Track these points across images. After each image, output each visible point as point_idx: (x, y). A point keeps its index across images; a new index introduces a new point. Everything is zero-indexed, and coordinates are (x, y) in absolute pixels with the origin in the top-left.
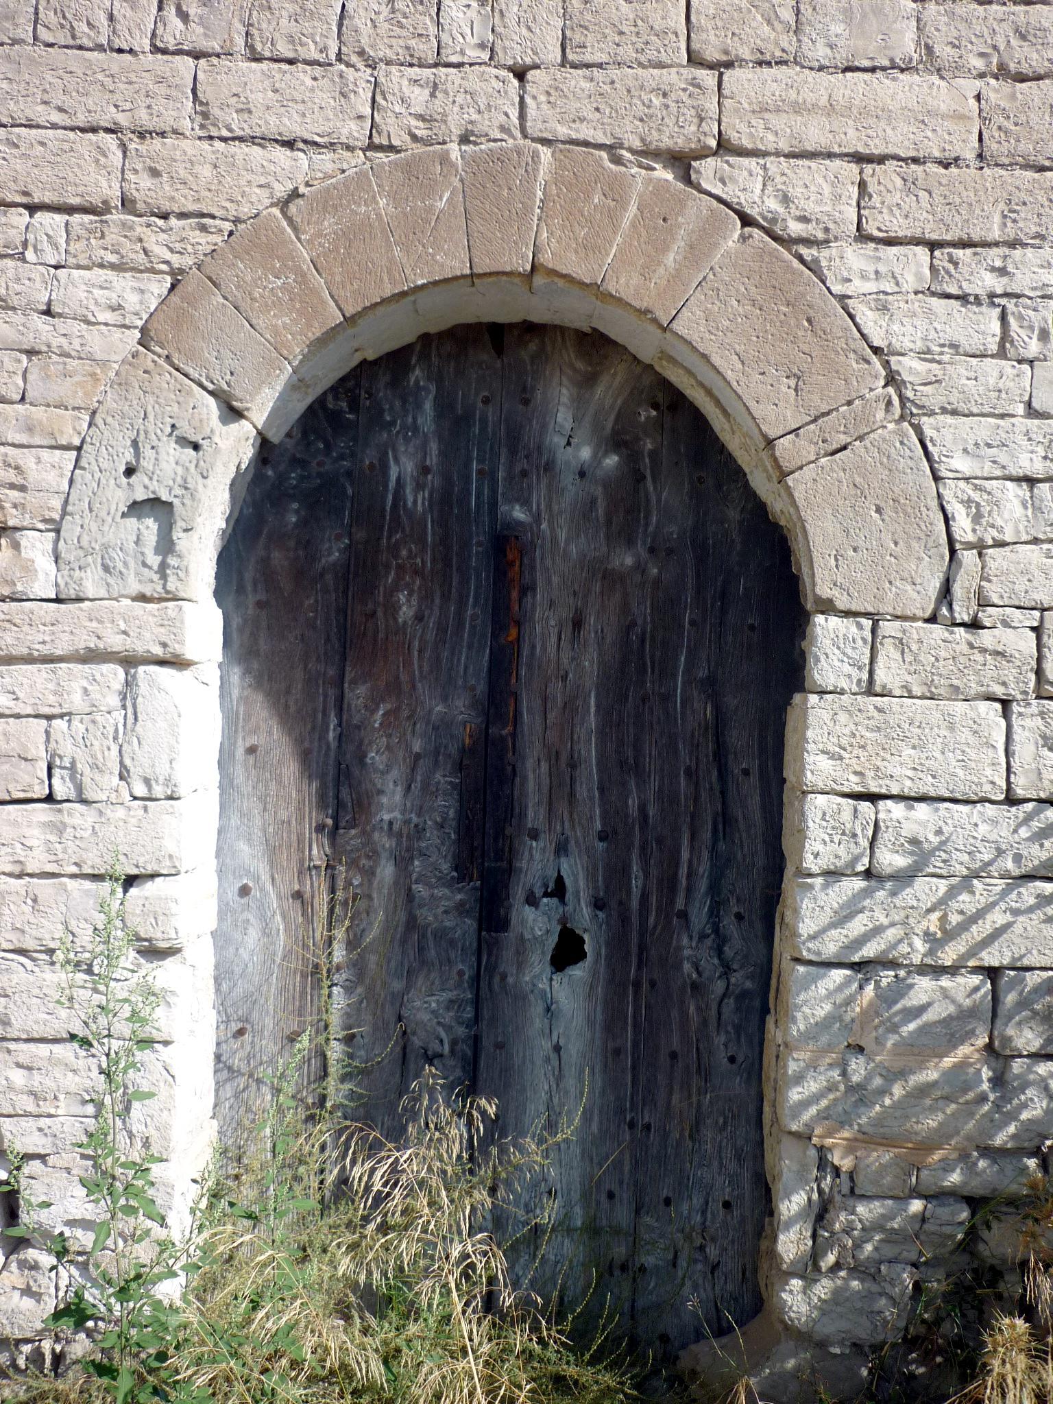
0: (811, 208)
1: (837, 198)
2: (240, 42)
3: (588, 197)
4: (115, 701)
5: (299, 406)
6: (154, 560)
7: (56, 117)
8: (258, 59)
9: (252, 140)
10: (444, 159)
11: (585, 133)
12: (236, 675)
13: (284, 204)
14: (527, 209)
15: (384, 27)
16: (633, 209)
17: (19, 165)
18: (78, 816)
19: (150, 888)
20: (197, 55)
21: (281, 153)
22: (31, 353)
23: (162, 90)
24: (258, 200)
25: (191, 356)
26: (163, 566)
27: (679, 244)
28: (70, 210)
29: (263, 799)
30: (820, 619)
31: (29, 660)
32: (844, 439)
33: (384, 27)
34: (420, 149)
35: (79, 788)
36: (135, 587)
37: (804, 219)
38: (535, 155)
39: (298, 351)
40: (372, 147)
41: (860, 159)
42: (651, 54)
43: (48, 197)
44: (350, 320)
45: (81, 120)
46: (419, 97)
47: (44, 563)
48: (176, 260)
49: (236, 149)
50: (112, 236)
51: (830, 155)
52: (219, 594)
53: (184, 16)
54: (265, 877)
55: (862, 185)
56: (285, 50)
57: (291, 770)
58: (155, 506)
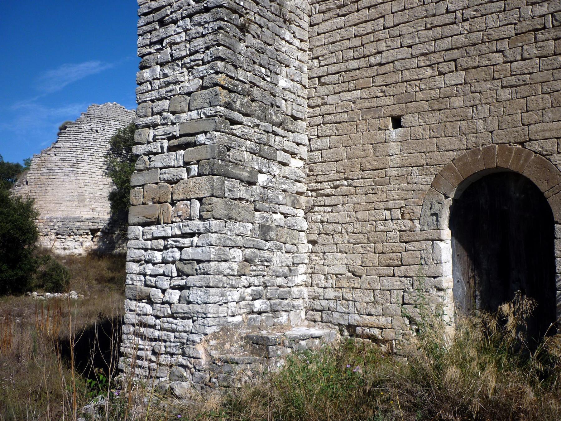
0: (548, 149)
1: (553, 146)
2: (443, 134)
3: (505, 153)
4: (430, 247)
5: (461, 193)
6: (435, 223)
7: (414, 151)
8: (446, 137)
9: (446, 151)
10: (479, 149)
11: (504, 141)
12: (455, 241)
13: (452, 161)
14: (494, 156)
15: (467, 128)
16: (513, 154)
17: (409, 160)
18: (426, 267)
19: (438, 278)
20: (436, 138)
21: (451, 152)
22: (413, 191)
23: (431, 145)
24: (448, 161)
25: (439, 188)
26: (437, 224)
27: (523, 159)
28: (418, 166)
29: (461, 264)
30: (556, 225)
31: (416, 241)
32: (557, 191)
33: (467, 128)
34: (474, 148)
35: (426, 262)
36: (433, 228)
37: (546, 151)
38: (495, 147)
39: (457, 185)
40: (467, 149)
41: (557, 138)
42: (515, 125)
43: (414, 165)
44: (465, 179)
45: (419, 151)
46: (474, 139)
47: (418, 225)
48: (435, 172)
49: (444, 153)
50: (425, 170)
51: (551, 138)
52: (450, 228)
53: (434, 132)
54: (462, 279)
55: (558, 143)
56: (450, 135)
57: (466, 259)
58: (435, 214)
